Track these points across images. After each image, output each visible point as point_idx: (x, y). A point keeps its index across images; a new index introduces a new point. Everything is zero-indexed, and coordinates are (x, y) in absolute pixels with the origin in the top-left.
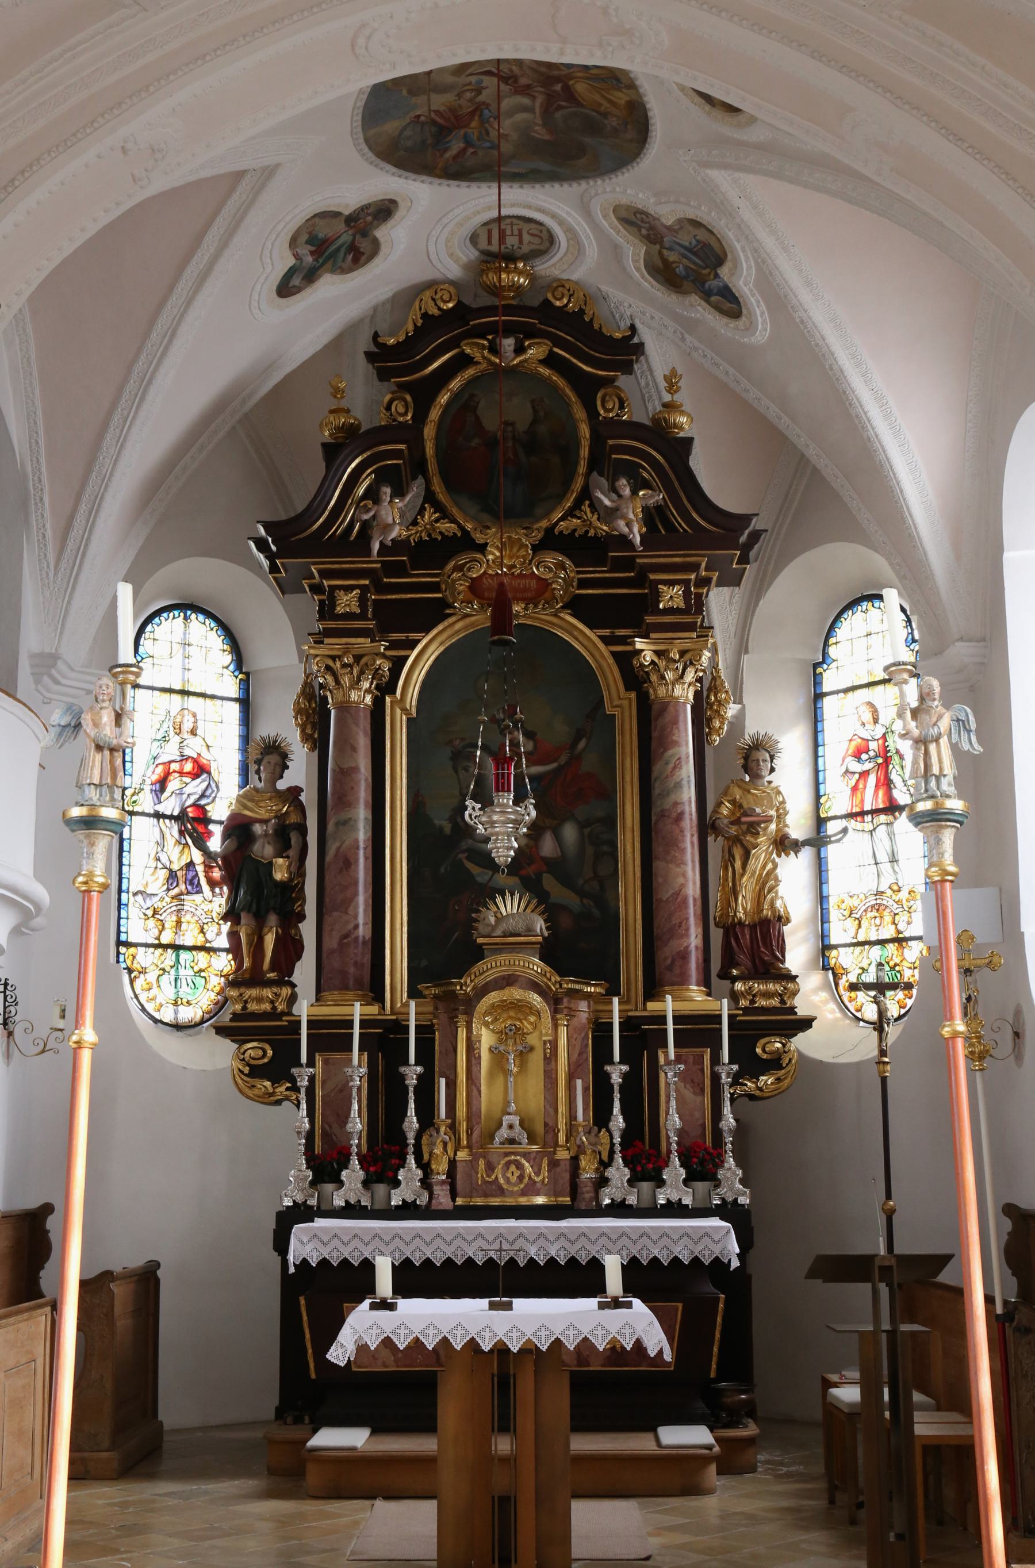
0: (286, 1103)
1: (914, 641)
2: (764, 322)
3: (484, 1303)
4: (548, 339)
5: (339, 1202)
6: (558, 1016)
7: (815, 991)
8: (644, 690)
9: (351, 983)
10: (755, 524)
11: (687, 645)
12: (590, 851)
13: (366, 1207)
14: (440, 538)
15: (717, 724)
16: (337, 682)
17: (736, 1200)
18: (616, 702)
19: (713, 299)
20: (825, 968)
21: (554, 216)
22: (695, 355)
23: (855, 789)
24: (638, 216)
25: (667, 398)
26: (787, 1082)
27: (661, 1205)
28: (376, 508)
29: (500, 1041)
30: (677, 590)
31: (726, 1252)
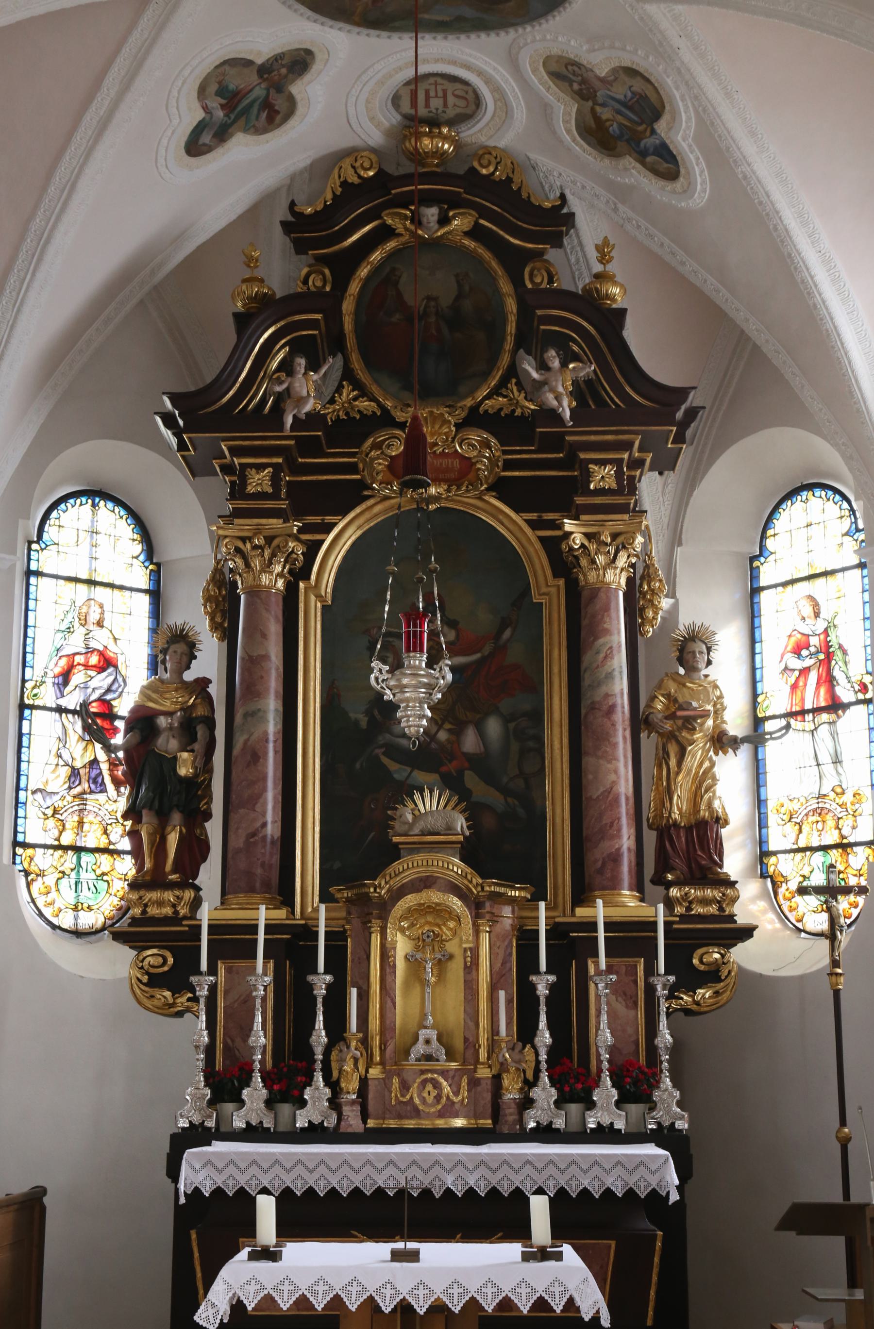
0: (188, 1016)
1: (858, 530)
2: (703, 182)
3: (384, 1249)
4: (473, 209)
5: (239, 1123)
6: (480, 922)
7: (753, 900)
8: (574, 576)
9: (258, 885)
10: (693, 399)
11: (621, 528)
12: (515, 746)
13: (269, 1128)
14: (358, 417)
15: (650, 614)
16: (247, 565)
17: (673, 1124)
18: (544, 590)
19: (649, 159)
20: (764, 876)
21: (480, 73)
22: (628, 227)
23: (794, 687)
24: (570, 68)
25: (598, 268)
26: (725, 997)
27: (591, 1129)
28: (289, 379)
29: (417, 948)
30: (609, 470)
31: (664, 1183)
